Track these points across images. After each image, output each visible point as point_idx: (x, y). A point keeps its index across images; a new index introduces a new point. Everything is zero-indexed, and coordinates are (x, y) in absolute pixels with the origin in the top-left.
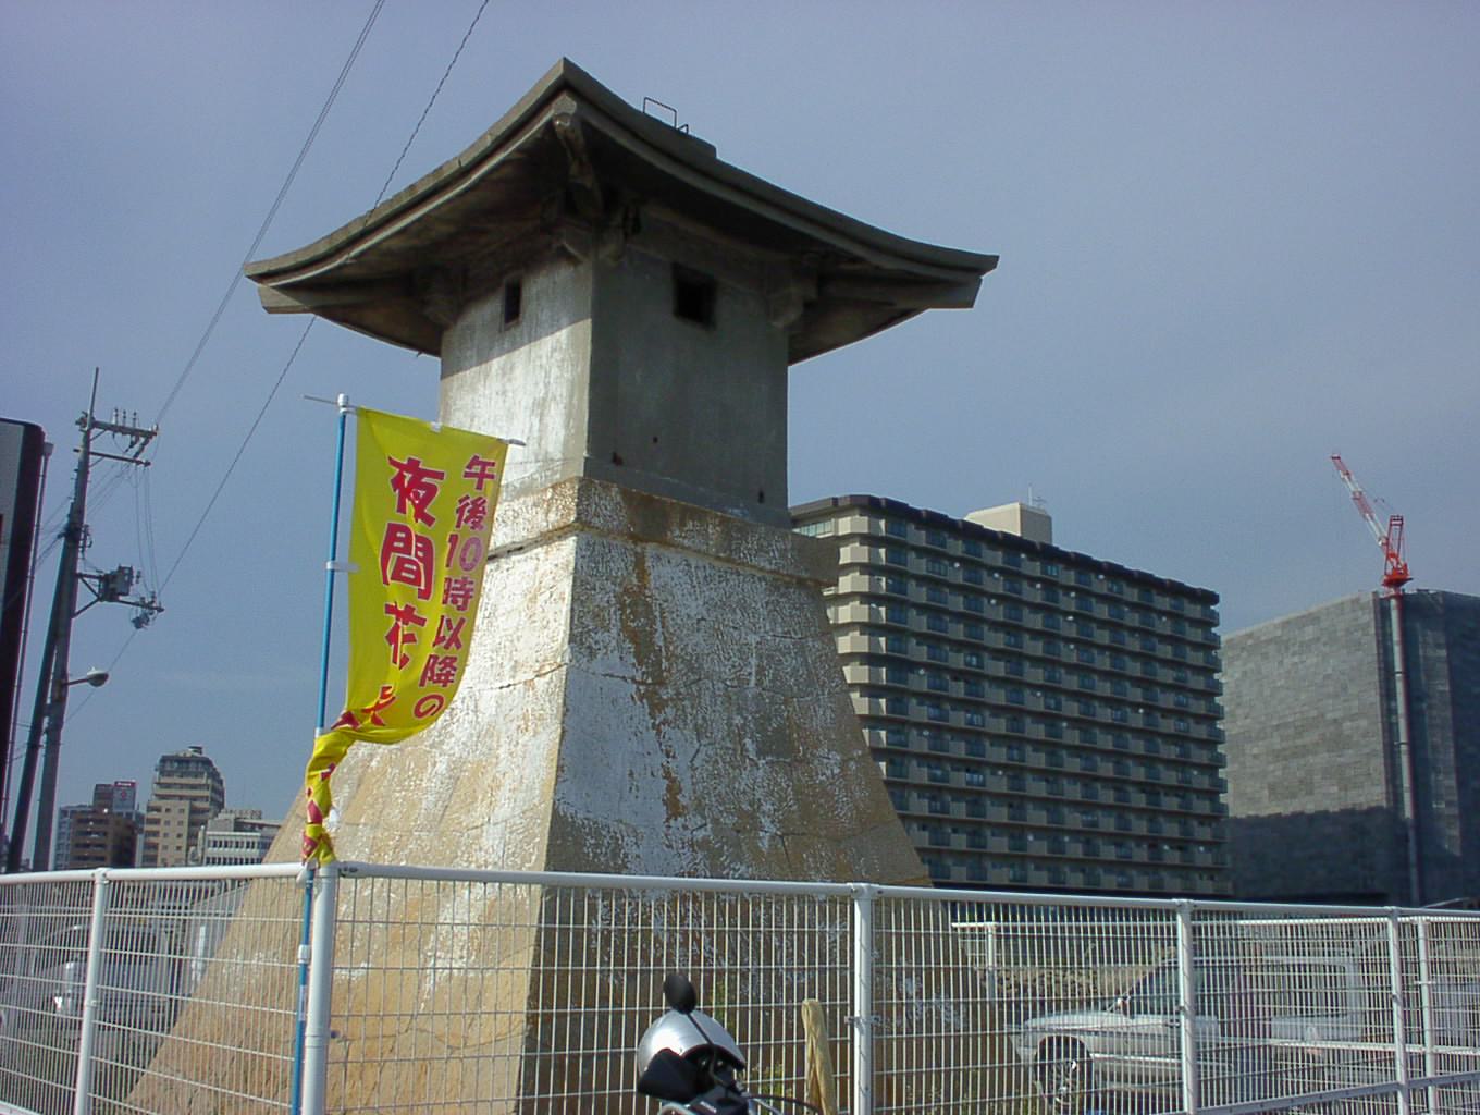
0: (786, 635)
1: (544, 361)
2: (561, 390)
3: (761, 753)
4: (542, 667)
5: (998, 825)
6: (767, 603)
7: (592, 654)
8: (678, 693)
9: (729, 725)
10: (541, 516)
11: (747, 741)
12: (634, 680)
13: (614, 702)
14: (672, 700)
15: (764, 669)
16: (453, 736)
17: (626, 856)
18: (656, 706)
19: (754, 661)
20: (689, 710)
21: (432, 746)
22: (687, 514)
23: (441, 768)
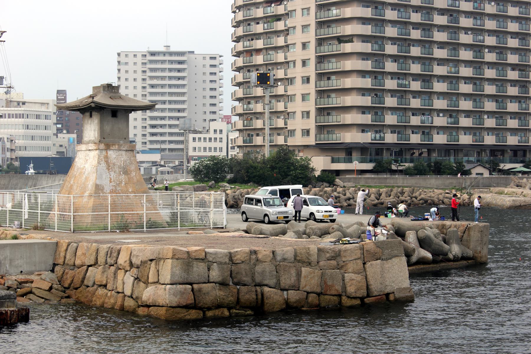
2: (97, 129)
3: (123, 174)
5: (441, 26)
18: (108, 169)
22: (113, 145)
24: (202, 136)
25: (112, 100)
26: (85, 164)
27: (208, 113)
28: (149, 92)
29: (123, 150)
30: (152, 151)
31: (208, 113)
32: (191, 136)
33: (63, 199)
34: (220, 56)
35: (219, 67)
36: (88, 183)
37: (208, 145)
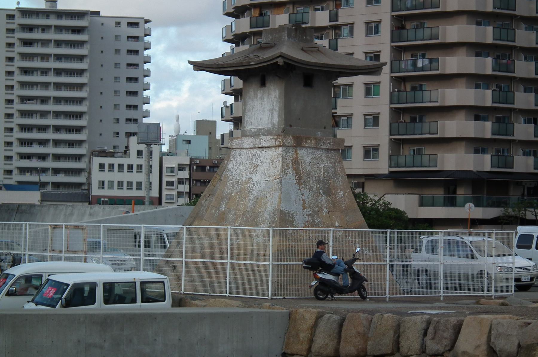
0: (331, 163)
1: (272, 99)
2: (277, 108)
3: (324, 193)
4: (276, 177)
6: (326, 156)
7: (287, 174)
8: (305, 181)
9: (317, 187)
10: (274, 142)
11: (321, 190)
12: (295, 179)
13: (291, 185)
14: (304, 183)
15: (325, 173)
16: (254, 190)
17: (295, 218)
18: (299, 183)
19: (322, 171)
20: (307, 185)
21: (249, 192)
23: (252, 197)
24: (116, 161)
25: (305, 54)
26: (251, 173)
27: (122, 120)
28: (19, 82)
29: (323, 149)
30: (22, 186)
31: (122, 120)
32: (96, 161)
33: (204, 239)
34: (147, 21)
35: (143, 40)
36: (263, 209)
37: (126, 177)
